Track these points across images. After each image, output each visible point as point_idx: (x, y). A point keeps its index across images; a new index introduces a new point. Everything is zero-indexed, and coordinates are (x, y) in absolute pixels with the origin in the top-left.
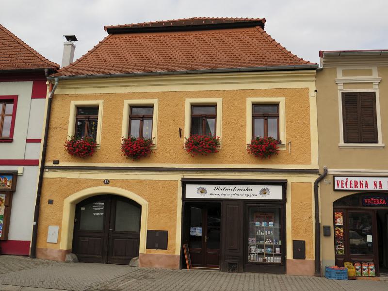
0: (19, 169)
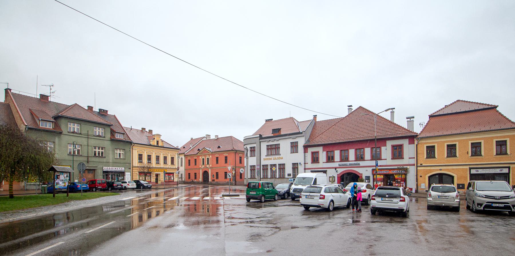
0: (408, 167)
